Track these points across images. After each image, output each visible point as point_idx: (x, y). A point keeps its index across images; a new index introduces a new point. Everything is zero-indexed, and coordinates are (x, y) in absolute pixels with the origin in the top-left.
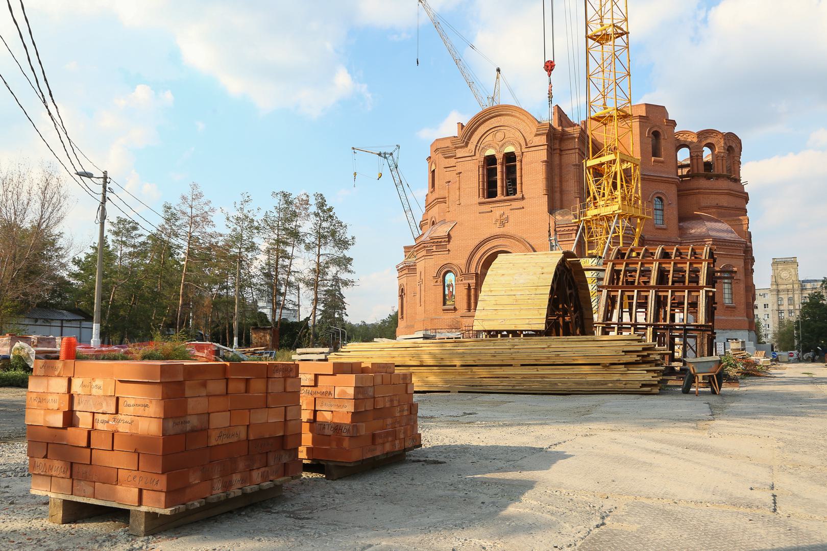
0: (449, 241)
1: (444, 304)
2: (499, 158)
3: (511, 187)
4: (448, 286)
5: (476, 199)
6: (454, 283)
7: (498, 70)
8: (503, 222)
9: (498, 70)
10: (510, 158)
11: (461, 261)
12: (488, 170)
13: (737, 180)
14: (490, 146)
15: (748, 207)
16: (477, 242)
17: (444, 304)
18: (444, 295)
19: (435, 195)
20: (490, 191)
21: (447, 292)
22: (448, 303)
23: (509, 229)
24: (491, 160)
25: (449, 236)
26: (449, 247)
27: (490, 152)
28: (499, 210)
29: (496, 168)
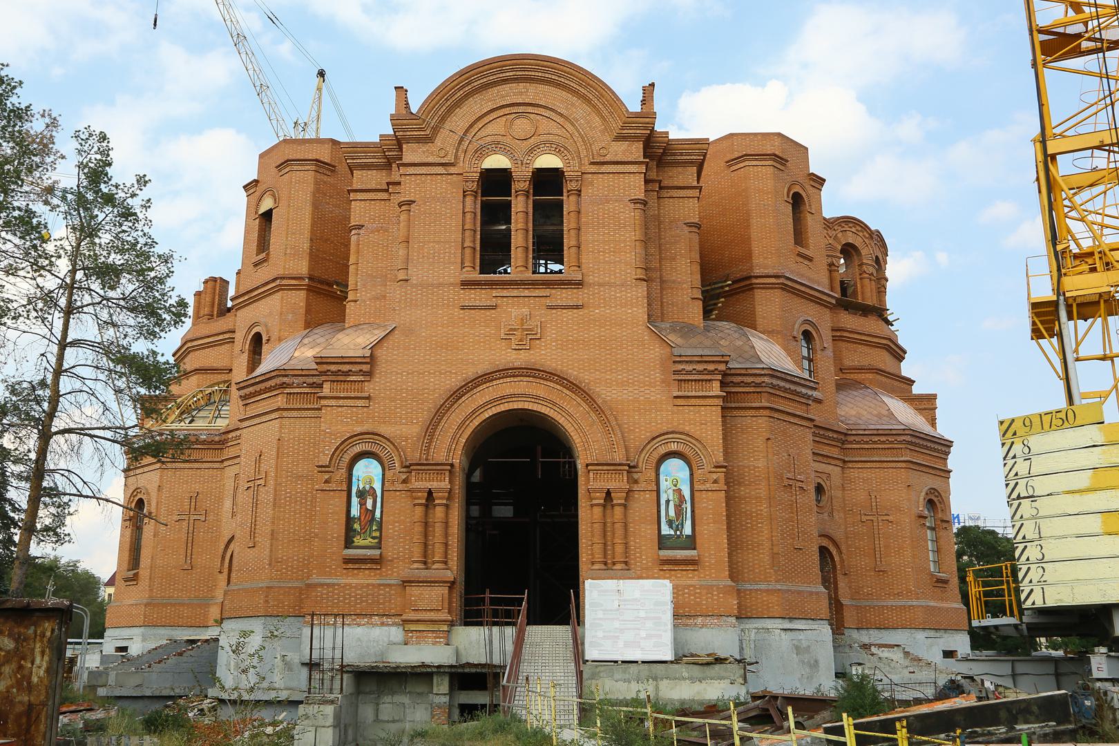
0: (370, 374)
1: (348, 543)
2: (521, 182)
3: (549, 246)
4: (362, 494)
5: (453, 273)
6: (377, 486)
7: (321, 74)
8: (529, 336)
9: (321, 74)
10: (548, 183)
11: (405, 429)
12: (484, 206)
13: (879, 312)
14: (497, 147)
15: (951, 463)
16: (455, 382)
17: (348, 543)
18: (349, 519)
19: (265, 274)
20: (493, 251)
21: (355, 511)
22: (358, 541)
23: (545, 355)
24: (495, 182)
25: (372, 360)
26: (369, 388)
27: (496, 161)
28: (516, 309)
29: (507, 234)
